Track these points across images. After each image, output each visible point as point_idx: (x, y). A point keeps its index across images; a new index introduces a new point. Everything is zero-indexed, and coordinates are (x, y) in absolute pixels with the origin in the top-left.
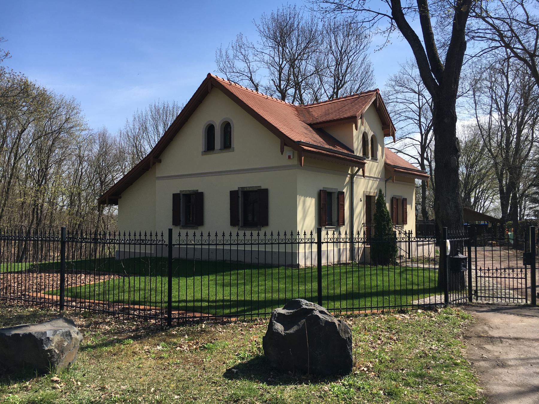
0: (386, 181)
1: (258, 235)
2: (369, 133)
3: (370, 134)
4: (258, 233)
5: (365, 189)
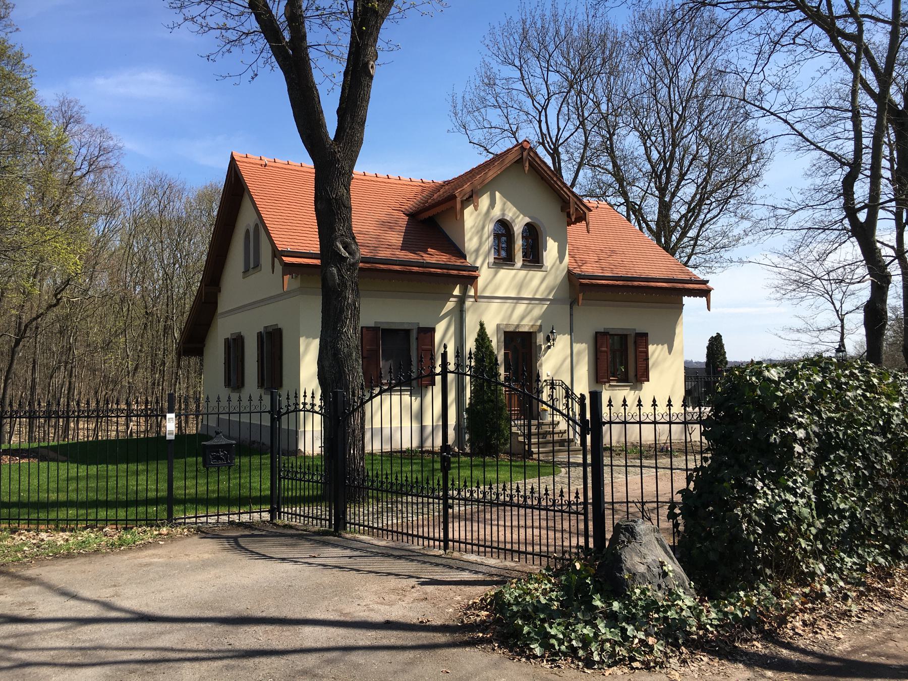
0: (573, 303)
1: (240, 400)
2: (517, 221)
3: (519, 225)
4: (240, 397)
5: (503, 320)
